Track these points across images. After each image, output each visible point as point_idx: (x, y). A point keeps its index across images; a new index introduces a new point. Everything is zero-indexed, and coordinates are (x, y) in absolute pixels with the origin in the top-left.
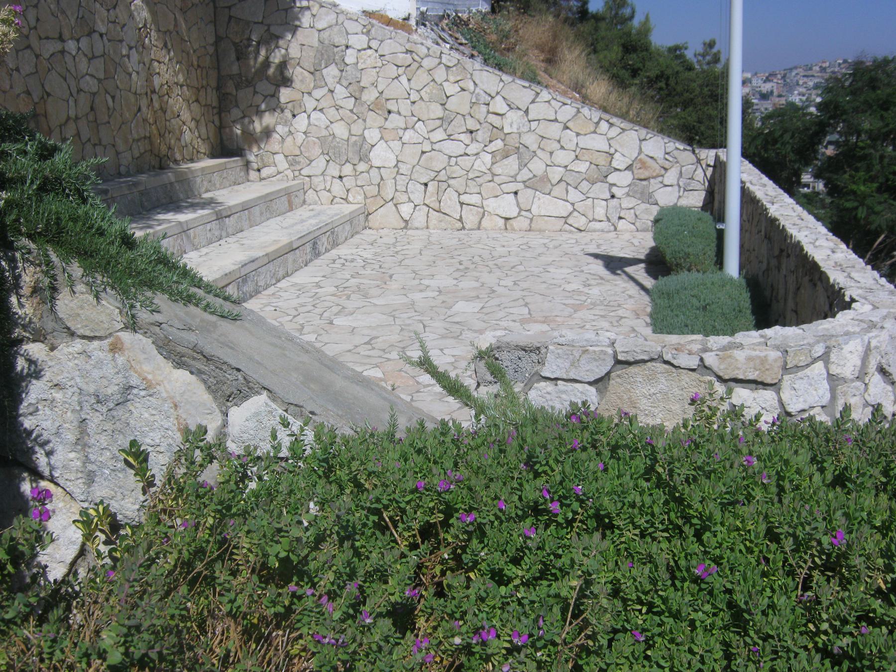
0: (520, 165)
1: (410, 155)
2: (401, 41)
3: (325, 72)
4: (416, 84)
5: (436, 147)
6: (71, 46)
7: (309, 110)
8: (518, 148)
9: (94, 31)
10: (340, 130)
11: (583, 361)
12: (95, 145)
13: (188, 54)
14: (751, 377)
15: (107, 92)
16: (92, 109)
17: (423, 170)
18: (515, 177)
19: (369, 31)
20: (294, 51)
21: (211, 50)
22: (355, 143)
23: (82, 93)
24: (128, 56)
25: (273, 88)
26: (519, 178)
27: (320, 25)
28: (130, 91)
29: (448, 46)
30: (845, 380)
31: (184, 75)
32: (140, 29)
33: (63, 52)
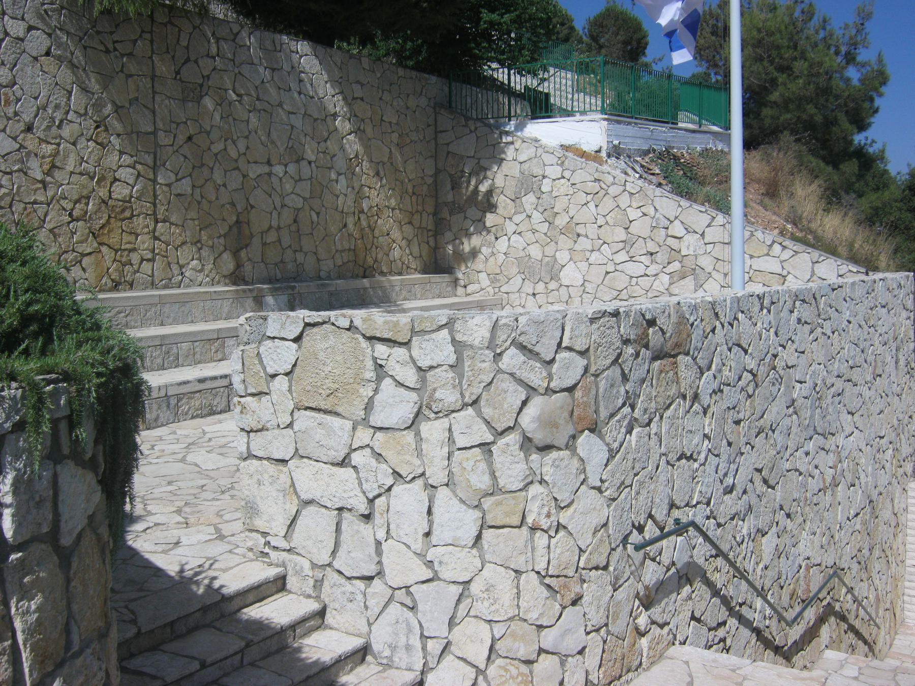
0: (696, 285)
1: (596, 275)
2: (590, 171)
3: (524, 199)
4: (603, 210)
5: (618, 267)
6: (279, 170)
7: (509, 234)
8: (694, 270)
9: (303, 159)
10: (535, 252)
11: (287, 324)
12: (295, 251)
13: (402, 183)
14: (386, 336)
15: (311, 209)
16: (295, 221)
17: (606, 289)
19: (563, 162)
20: (499, 182)
21: (430, 181)
22: (547, 264)
23: (286, 208)
24: (337, 181)
25: (480, 213)
27: (522, 158)
28: (336, 209)
29: (637, 176)
30: (471, 346)
31: (396, 199)
32: (351, 159)
33: (270, 174)
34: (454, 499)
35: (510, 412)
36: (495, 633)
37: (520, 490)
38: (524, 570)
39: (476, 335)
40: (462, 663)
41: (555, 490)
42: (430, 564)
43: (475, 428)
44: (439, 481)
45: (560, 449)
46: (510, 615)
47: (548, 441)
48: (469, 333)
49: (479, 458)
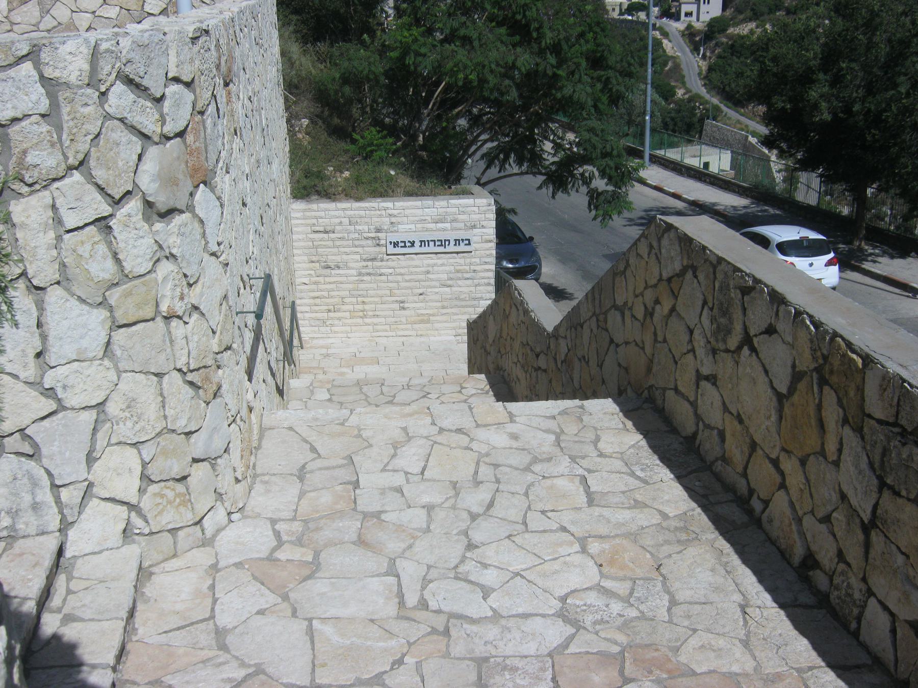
0: (41, 11)
18: (37, 25)
26: (42, 26)
30: (67, 85)
34: (71, 299)
35: (126, 172)
36: (144, 456)
37: (149, 272)
38: (166, 371)
39: (71, 68)
40: (109, 505)
41: (184, 265)
42: (49, 393)
43: (87, 199)
44: (48, 279)
45: (181, 212)
46: (158, 430)
47: (171, 204)
48: (61, 65)
49: (96, 239)
